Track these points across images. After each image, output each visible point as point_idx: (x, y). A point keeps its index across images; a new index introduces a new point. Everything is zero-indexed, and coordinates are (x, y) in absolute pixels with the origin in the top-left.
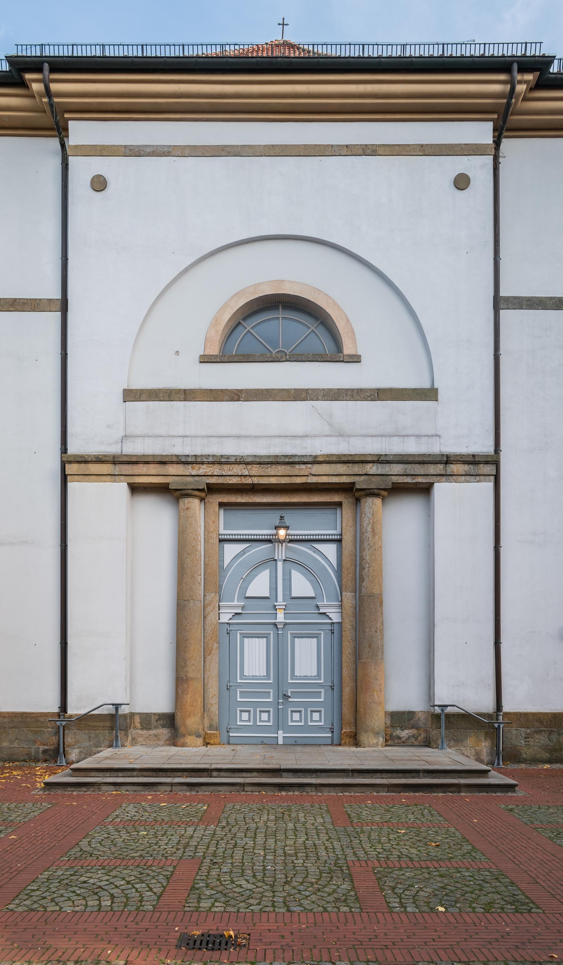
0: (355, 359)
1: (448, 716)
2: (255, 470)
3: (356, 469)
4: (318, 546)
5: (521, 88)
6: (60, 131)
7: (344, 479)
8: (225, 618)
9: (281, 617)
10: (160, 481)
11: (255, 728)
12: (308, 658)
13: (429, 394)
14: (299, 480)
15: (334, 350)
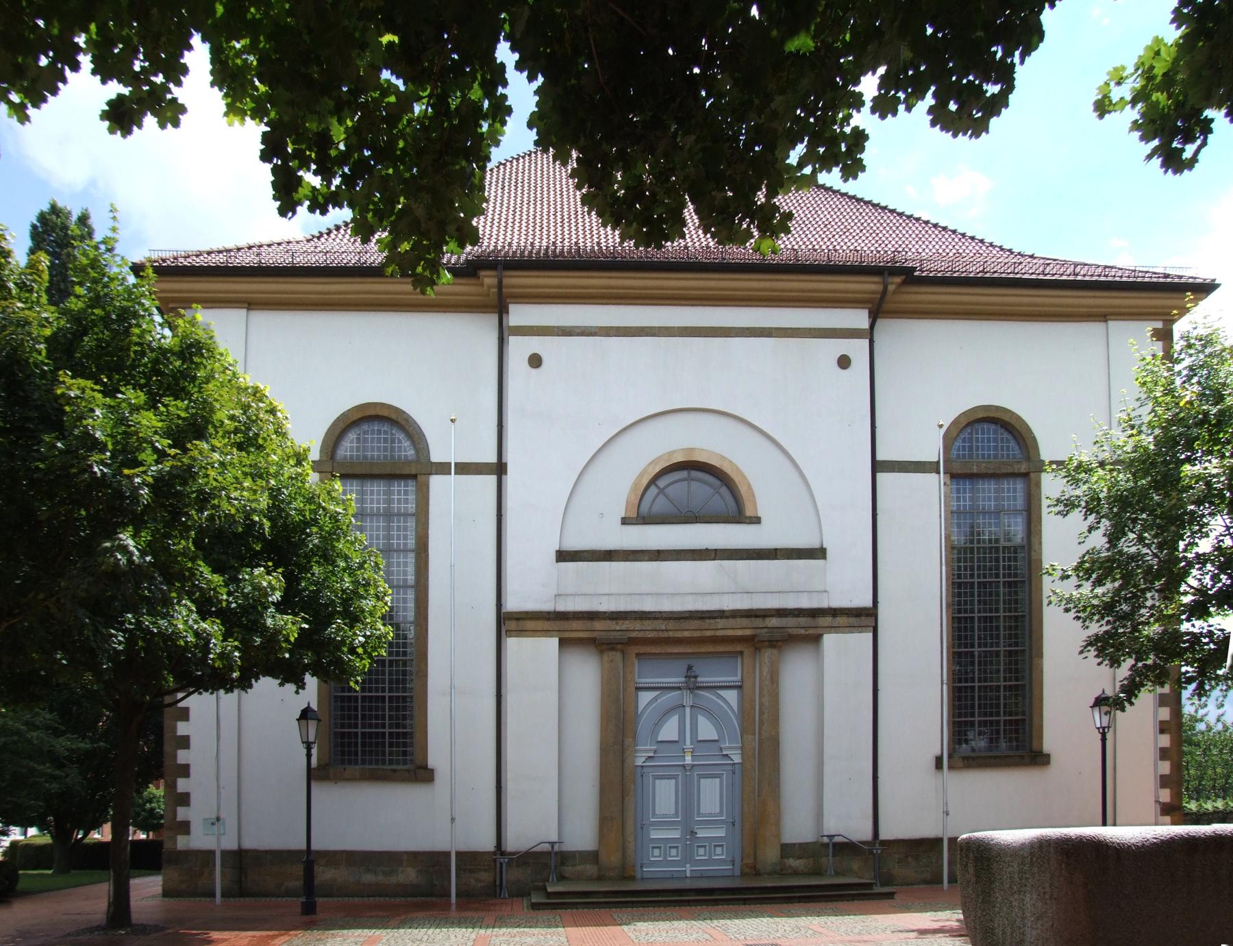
0: (756, 520)
1: (835, 845)
2: (671, 625)
3: (759, 622)
4: (721, 692)
5: (891, 288)
6: (501, 310)
7: (748, 632)
8: (639, 762)
9: (688, 760)
10: (577, 630)
11: (666, 863)
12: (712, 796)
13: (818, 553)
14: (708, 633)
15: (739, 514)
